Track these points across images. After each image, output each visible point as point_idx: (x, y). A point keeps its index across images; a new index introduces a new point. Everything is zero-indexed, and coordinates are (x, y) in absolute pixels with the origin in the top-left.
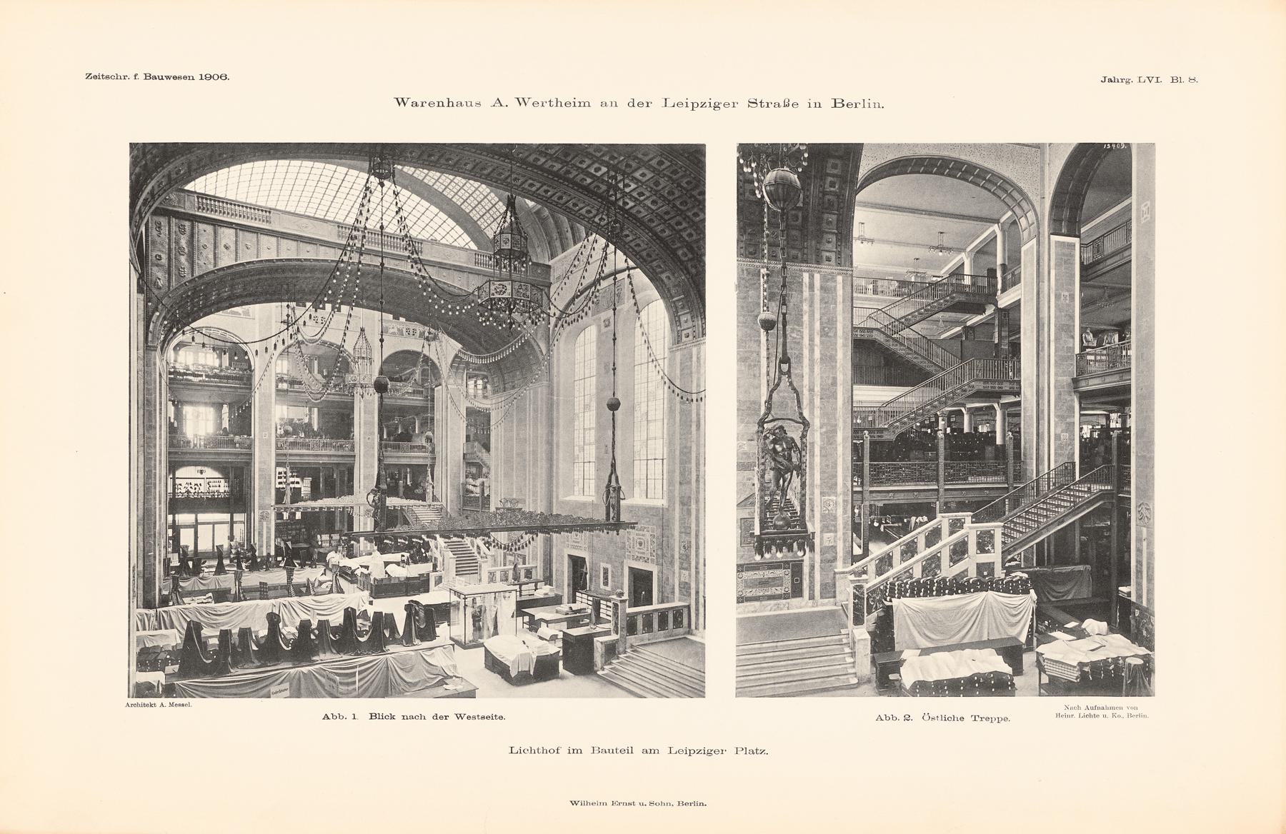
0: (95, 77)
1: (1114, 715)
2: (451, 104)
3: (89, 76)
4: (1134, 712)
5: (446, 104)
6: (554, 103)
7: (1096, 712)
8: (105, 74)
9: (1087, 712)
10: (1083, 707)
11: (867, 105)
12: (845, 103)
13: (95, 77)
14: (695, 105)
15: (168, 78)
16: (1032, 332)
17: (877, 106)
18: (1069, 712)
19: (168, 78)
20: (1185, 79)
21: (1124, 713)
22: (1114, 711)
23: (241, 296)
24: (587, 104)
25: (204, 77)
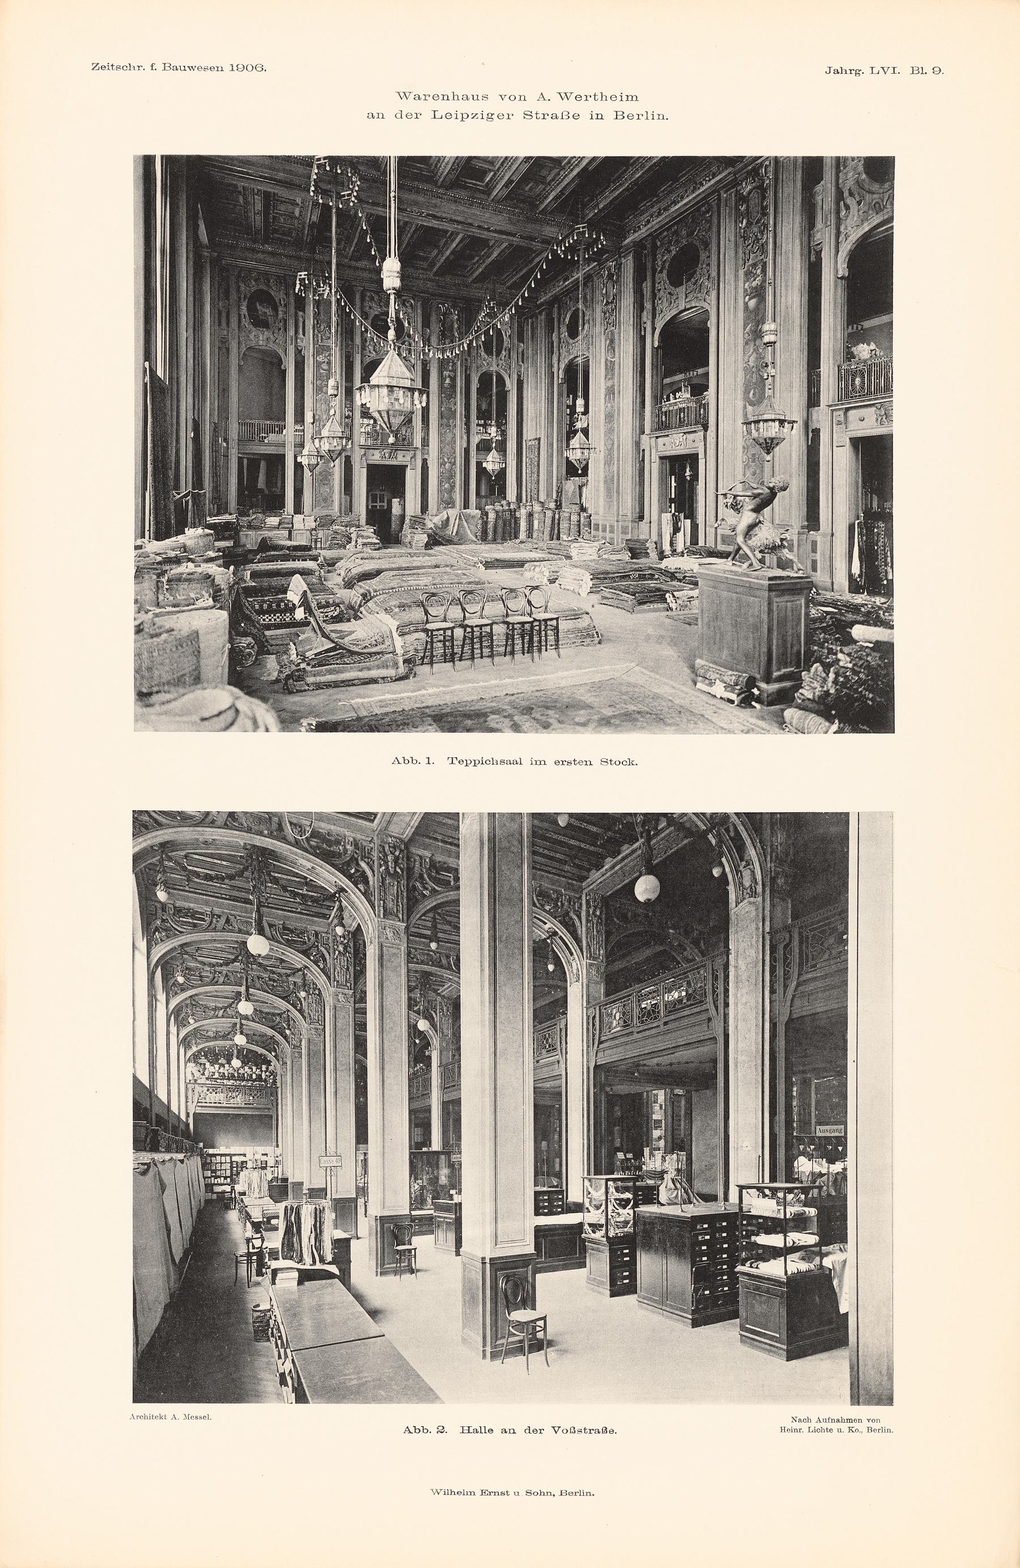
0: (103, 68)
1: (850, 1429)
2: (456, 97)
3: (95, 66)
4: (875, 1426)
5: (451, 98)
6: (599, 97)
7: (830, 1425)
8: (115, 65)
9: (818, 1426)
10: (814, 1419)
11: (650, 117)
12: (625, 115)
13: (103, 68)
14: (465, 116)
15: (191, 68)
16: (736, 1059)
17: (661, 117)
18: (797, 1425)
19: (191, 68)
20: (928, 69)
21: (862, 1427)
22: (851, 1425)
23: (709, 195)
24: (543, 763)
25: (235, 68)
